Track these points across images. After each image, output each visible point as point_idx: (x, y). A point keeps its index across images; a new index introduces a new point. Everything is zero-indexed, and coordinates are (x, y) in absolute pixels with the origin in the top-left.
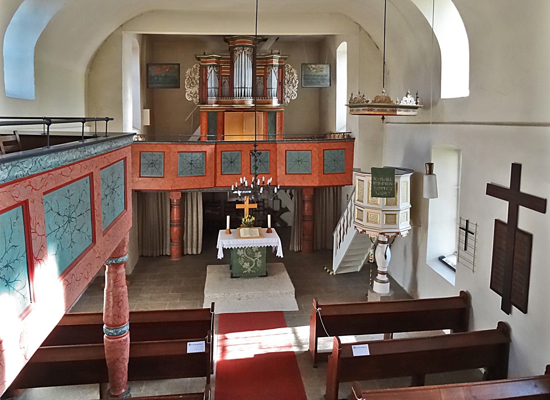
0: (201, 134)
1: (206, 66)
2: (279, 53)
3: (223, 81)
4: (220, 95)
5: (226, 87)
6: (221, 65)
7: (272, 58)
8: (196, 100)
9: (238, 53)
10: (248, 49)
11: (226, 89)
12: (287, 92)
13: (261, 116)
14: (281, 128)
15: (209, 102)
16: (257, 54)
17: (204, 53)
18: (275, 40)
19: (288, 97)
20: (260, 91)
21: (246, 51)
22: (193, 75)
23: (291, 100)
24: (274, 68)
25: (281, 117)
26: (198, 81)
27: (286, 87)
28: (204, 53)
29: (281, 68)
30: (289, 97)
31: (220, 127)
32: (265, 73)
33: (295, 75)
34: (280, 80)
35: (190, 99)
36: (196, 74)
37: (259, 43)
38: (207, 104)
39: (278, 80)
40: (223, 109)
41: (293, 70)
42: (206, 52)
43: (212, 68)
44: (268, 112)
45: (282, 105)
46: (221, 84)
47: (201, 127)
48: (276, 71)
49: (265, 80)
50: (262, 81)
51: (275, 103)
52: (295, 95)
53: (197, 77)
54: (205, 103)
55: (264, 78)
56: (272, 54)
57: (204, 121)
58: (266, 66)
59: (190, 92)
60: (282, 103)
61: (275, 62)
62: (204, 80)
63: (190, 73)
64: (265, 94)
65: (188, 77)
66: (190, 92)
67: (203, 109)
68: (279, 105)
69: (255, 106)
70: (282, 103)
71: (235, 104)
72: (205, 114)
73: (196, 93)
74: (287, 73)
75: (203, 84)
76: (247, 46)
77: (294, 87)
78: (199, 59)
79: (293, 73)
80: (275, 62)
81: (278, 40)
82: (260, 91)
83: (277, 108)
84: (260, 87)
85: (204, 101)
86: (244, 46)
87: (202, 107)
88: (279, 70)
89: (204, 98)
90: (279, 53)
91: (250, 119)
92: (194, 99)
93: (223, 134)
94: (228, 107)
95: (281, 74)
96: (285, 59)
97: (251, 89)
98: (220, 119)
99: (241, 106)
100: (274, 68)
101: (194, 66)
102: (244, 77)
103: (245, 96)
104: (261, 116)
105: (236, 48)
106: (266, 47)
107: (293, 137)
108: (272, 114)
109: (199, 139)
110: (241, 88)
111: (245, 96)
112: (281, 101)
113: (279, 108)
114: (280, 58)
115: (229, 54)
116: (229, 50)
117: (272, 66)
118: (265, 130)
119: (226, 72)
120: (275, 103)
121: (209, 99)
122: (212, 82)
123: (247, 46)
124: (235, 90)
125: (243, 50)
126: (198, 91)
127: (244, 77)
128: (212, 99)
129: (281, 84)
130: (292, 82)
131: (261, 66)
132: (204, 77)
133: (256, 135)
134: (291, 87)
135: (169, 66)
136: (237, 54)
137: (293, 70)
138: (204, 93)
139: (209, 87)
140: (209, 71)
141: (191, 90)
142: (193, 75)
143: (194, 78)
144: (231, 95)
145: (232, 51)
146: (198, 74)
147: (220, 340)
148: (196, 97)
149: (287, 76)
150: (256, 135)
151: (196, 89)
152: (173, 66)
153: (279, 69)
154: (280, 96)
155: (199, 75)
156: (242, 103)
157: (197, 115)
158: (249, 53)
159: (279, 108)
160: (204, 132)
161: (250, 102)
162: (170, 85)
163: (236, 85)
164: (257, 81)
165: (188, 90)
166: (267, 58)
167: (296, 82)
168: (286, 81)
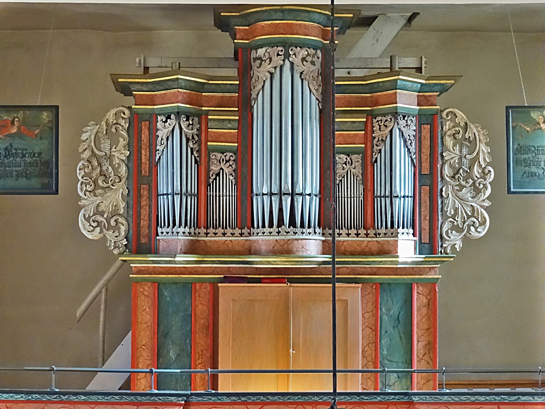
0: (134, 363)
1: (152, 117)
2: (419, 70)
3: (215, 168)
4: (203, 218)
5: (226, 193)
6: (207, 113)
7: (394, 86)
8: (117, 238)
9: (267, 67)
10: (303, 53)
11: (227, 206)
12: (450, 211)
13: (353, 296)
14: (431, 347)
15: (162, 245)
16: (338, 73)
17: (146, 69)
18: (404, 22)
19: (455, 228)
20: (349, 212)
21: (297, 61)
22: (106, 145)
23: (466, 240)
24: (402, 122)
25: (431, 304)
26: (123, 170)
27: (448, 191)
28: (146, 69)
29: (429, 121)
30: (459, 230)
31: (201, 341)
32: (369, 139)
33: (483, 148)
34: (426, 166)
35: (95, 235)
36: (114, 143)
37: (342, 31)
38: (156, 252)
39: (417, 166)
40: (213, 271)
41: (474, 130)
42: (152, 62)
43: (173, 121)
44: (381, 285)
45: (433, 258)
46: (206, 181)
47: (134, 338)
48: (410, 131)
49: (368, 164)
50: (358, 171)
51: (407, 249)
52: (483, 223)
53: (121, 153)
54: (151, 249)
55: (364, 159)
56: (392, 71)
57: (146, 315)
58: (371, 115)
59: (97, 208)
60: (432, 251)
61: (406, 101)
62: (145, 168)
63: (93, 142)
64: (372, 217)
65: (87, 154)
66: (97, 208)
67: (139, 271)
68: (420, 258)
69: (333, 263)
70: (432, 251)
71: (257, 253)
72: (148, 289)
73: (115, 213)
74: (449, 142)
75: (142, 178)
76: (301, 45)
77: (477, 191)
78: (125, 90)
79: (472, 143)
80: (406, 101)
81: (414, 22)
82: (349, 212)
83: (413, 269)
84: (350, 194)
85: (141, 243)
86: (287, 45)
87: (138, 262)
88: (419, 131)
89: (144, 231)
90: (419, 70)
91: (313, 309)
92: (109, 234)
93: (214, 364)
94: (233, 264)
95: (426, 143)
96: (444, 89)
97: (316, 201)
98: (202, 308)
99: (279, 262)
100: (402, 122)
101: (110, 116)
102: (291, 158)
103: (292, 223)
104: (353, 296)
105: (261, 52)
106: (368, 48)
107: (475, 378)
108: (400, 287)
109: (127, 385)
110: (281, 194)
111: (292, 223)
112: (429, 245)
113: (420, 272)
114: (423, 88)
115: (233, 72)
116: (236, 58)
117: (395, 114)
118: (370, 352)
119: (223, 127)
120: (407, 249)
121: (165, 236)
122: (173, 175)
123: (301, 45)
124: (257, 202)
125: (287, 56)
126: (122, 205)
127: (291, 158)
128: (173, 237)
129: (428, 179)
130: (469, 175)
131: (350, 109)
132: (144, 153)
133: (335, 372)
134: (466, 193)
135: (21, 114)
136: (261, 73)
137: (474, 130)
138: (144, 212)
139: (162, 189)
140: (162, 133)
141: (98, 200)
142: (106, 145)
143: (110, 158)
144: (246, 220)
145: (243, 60)
146: (122, 142)
147: (250, 247)
148: (116, 228)
149: (452, 152)
150: (335, 372)
151: (116, 198)
152: (34, 112)
153: (420, 125)
154: (426, 225)
155: (129, 146)
156: (285, 250)
157: (123, 290)
158: (307, 67)
159: (420, 272)
160: (145, 357)
161: (311, 247)
162: (23, 182)
163: (261, 184)
164: (340, 171)
165: (89, 203)
166: (372, 88)
167: (484, 174)
168: (447, 171)
